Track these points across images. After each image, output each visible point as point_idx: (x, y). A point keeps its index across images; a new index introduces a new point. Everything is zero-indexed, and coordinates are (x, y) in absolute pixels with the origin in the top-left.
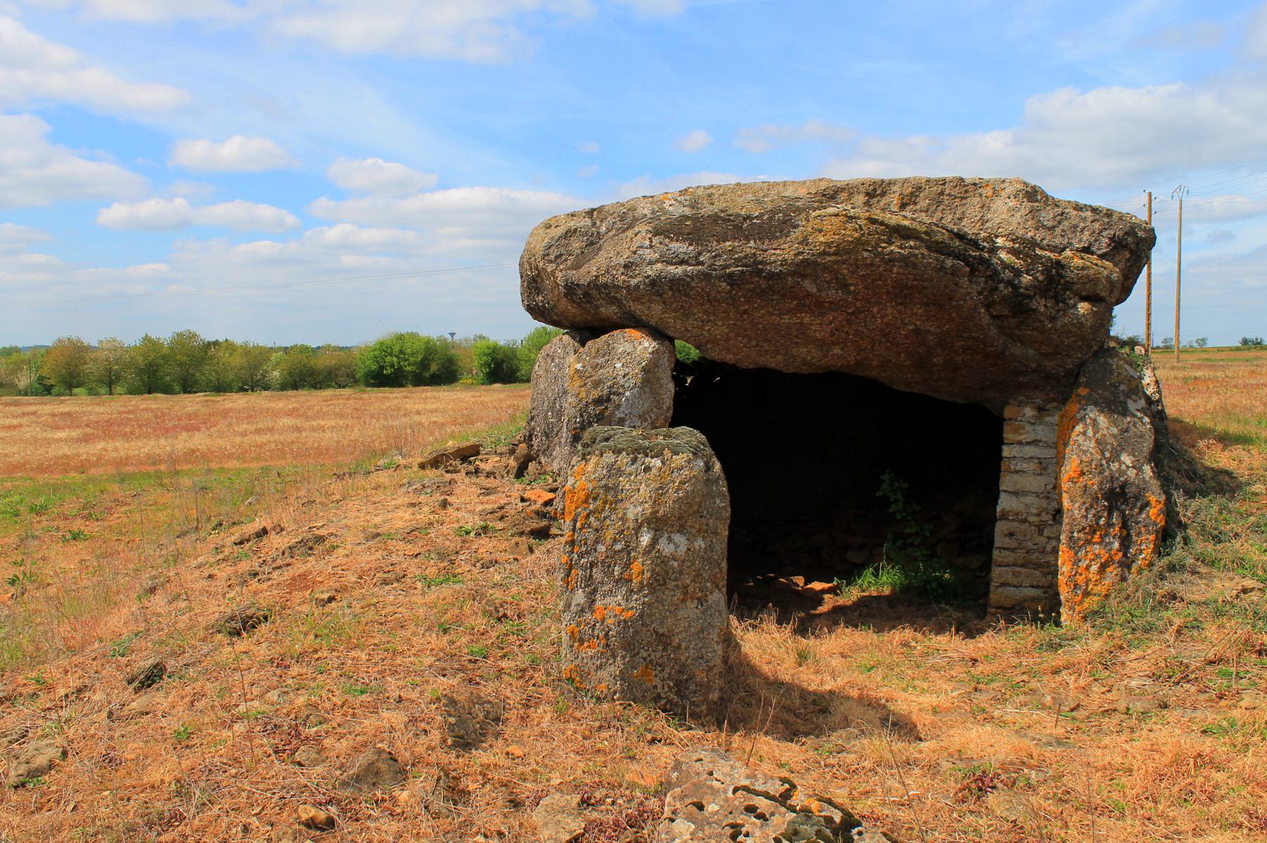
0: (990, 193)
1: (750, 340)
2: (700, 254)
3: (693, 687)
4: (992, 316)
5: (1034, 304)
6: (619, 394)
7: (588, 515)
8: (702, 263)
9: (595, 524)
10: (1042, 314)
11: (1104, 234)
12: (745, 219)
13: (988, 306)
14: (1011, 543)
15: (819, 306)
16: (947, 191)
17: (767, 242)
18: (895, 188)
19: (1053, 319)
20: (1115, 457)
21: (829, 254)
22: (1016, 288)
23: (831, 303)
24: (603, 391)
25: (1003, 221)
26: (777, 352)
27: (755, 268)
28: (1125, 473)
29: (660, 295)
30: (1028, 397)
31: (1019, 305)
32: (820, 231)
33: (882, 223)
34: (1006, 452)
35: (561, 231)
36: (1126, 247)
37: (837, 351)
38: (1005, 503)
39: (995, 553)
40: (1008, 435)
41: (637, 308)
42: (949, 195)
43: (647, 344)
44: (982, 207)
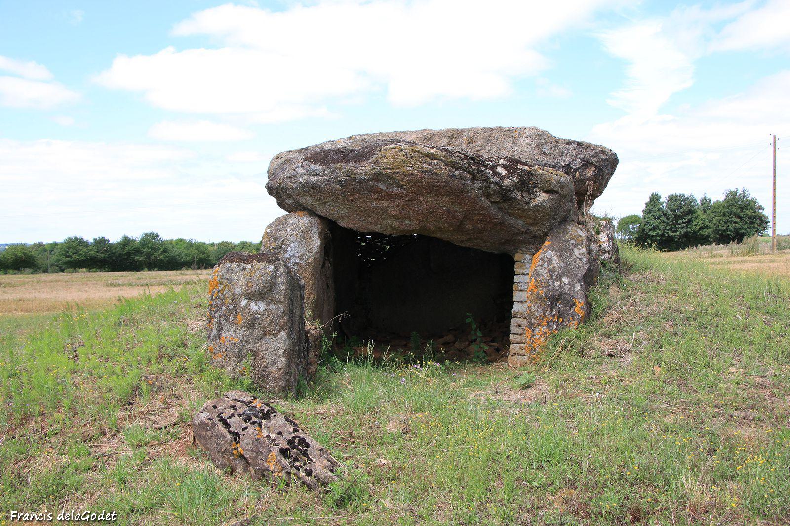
0: (517, 135)
1: (361, 217)
2: (325, 170)
3: (270, 378)
4: (492, 202)
5: (513, 195)
6: (287, 245)
7: (218, 292)
8: (326, 175)
9: (222, 297)
10: (521, 201)
11: (578, 157)
12: (351, 151)
13: (488, 196)
14: (519, 330)
15: (389, 197)
16: (494, 135)
17: (358, 163)
18: (464, 134)
19: (528, 203)
20: (559, 278)
21: (389, 169)
22: (501, 186)
23: (395, 195)
24: (279, 243)
25: (327, 147)
26: (377, 224)
27: (352, 178)
28: (562, 287)
29: (308, 192)
30: (527, 248)
31: (504, 196)
32: (385, 157)
33: (419, 152)
34: (516, 279)
35: (282, 160)
36: (592, 164)
37: (407, 222)
38: (516, 308)
39: (511, 336)
40: (517, 270)
41: (301, 200)
42: (494, 137)
43: (305, 219)
44: (513, 143)
